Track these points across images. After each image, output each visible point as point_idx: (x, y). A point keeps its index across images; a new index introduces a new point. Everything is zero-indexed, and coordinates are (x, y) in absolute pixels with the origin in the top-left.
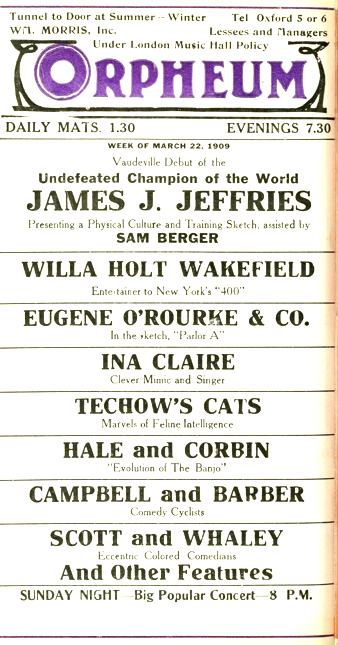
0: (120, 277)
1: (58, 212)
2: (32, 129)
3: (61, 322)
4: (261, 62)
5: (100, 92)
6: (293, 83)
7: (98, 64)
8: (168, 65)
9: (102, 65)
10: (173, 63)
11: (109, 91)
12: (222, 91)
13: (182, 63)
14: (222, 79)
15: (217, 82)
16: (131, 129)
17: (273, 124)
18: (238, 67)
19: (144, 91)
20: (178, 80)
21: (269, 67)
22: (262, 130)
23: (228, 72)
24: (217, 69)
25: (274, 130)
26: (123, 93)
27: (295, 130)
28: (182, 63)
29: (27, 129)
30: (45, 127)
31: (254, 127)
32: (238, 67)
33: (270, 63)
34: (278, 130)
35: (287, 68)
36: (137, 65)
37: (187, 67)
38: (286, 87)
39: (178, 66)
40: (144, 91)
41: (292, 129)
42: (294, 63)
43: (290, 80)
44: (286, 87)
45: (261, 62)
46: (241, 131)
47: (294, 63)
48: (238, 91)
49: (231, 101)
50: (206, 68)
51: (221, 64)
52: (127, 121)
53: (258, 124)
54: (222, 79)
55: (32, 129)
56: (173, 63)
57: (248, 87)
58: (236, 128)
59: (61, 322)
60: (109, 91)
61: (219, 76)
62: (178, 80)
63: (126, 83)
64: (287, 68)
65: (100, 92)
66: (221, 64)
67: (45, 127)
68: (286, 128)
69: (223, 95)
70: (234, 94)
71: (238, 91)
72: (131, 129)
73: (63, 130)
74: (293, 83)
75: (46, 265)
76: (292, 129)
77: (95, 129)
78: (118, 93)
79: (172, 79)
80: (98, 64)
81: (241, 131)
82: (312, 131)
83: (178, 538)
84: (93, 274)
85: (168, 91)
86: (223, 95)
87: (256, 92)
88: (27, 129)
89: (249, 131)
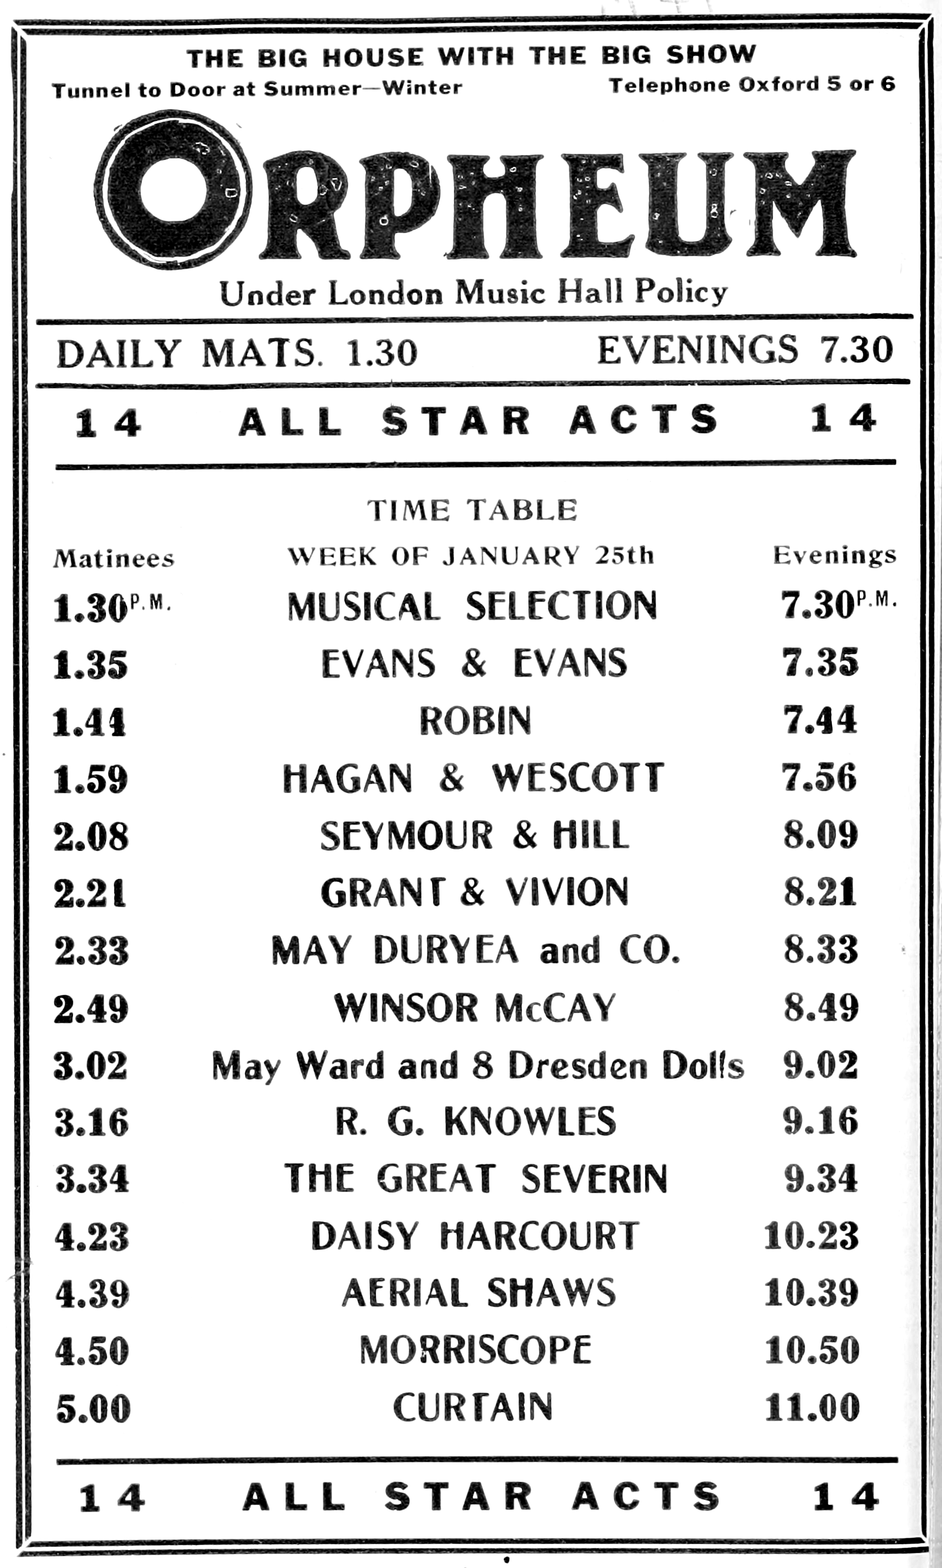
0: (121, 369)
1: (109, 369)
2: (129, 359)
3: (334, 899)
4: (727, 156)
5: (280, 246)
6: (817, 211)
7: (269, 165)
8: (467, 167)
9: (283, 170)
10: (483, 160)
11: (304, 241)
12: (621, 238)
13: (508, 161)
14: (617, 204)
15: (605, 212)
16: (407, 357)
17: (726, 340)
18: (662, 170)
19: (401, 240)
20: (495, 210)
21: (750, 167)
22: (697, 356)
23: (633, 185)
24: (605, 178)
25: (730, 355)
26: (344, 246)
27: (788, 355)
28: (508, 161)
29: (115, 359)
30: (168, 354)
31: (674, 347)
32: (662, 170)
33: (704, 156)
34: (740, 355)
35: (799, 169)
36: (379, 168)
37: (521, 174)
38: (797, 227)
39: (494, 170)
40: (401, 240)
41: (780, 352)
42: (820, 157)
43: (810, 205)
44: (797, 227)
45: (727, 156)
46: (636, 358)
47: (820, 157)
48: (665, 238)
49: (643, 261)
50: (574, 174)
51: (615, 162)
52: (397, 333)
53: (683, 340)
54: (617, 204)
55: (129, 359)
56: (483, 160)
57: (691, 226)
58: (621, 349)
59: (334, 899)
60: (304, 241)
61: (611, 196)
62: (495, 210)
63: (350, 221)
64: (799, 169)
65: (280, 246)
66: (615, 162)
67: (168, 354)
68: (762, 348)
69: (621, 249)
70: (652, 245)
71: (665, 238)
72: (407, 357)
73: (218, 360)
74: (817, 211)
75: (368, 1000)
76: (780, 352)
77: (304, 358)
78: (329, 247)
79: (479, 204)
80: (269, 165)
81: (636, 358)
82: (836, 356)
83: (486, 1008)
84: (514, 958)
85: (468, 242)
86: (621, 249)
87: (715, 240)
88: (115, 359)
89: (657, 360)
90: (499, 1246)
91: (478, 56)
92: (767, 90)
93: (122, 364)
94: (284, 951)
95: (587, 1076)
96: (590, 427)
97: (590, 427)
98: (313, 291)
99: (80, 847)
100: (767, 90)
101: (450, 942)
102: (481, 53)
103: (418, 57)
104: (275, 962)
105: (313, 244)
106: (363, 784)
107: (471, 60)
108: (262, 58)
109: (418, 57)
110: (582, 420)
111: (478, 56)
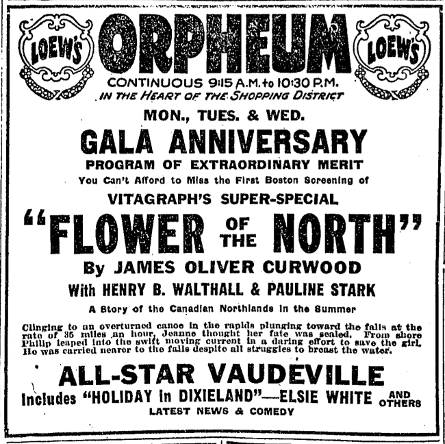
31: (271, 139)
90: (294, 168)
91: (125, 199)
92: (207, 168)
93: (205, 400)
94: (73, 290)
95: (230, 203)
96: (94, 312)
97: (94, 312)
98: (116, 272)
99: (301, 203)
100: (207, 168)
101: (301, 162)
102: (356, 164)
103: (253, 240)
104: (320, 168)
105: (362, 143)
106: (123, 269)
107: (121, 203)
108: (267, 180)
109: (253, 240)
110: (236, 374)
111: (125, 199)
